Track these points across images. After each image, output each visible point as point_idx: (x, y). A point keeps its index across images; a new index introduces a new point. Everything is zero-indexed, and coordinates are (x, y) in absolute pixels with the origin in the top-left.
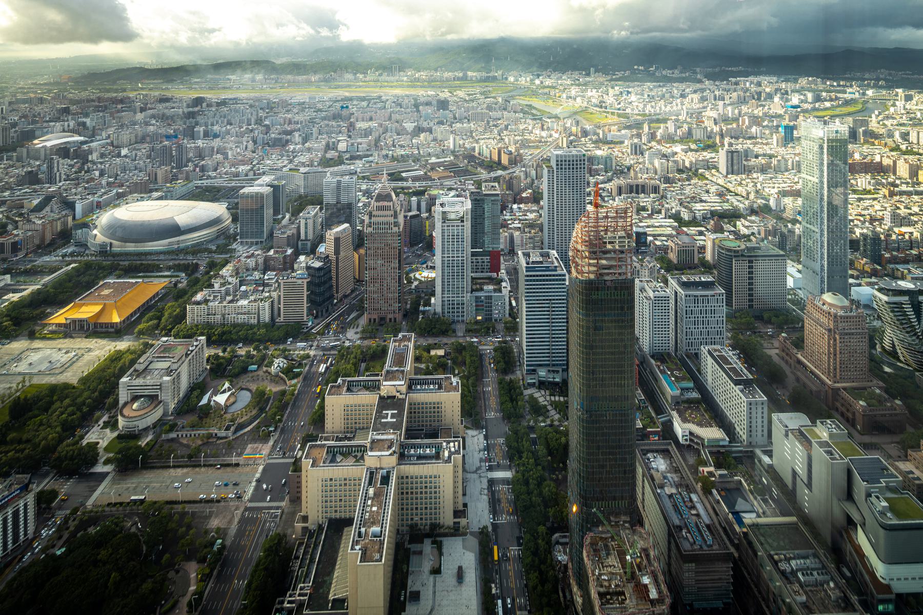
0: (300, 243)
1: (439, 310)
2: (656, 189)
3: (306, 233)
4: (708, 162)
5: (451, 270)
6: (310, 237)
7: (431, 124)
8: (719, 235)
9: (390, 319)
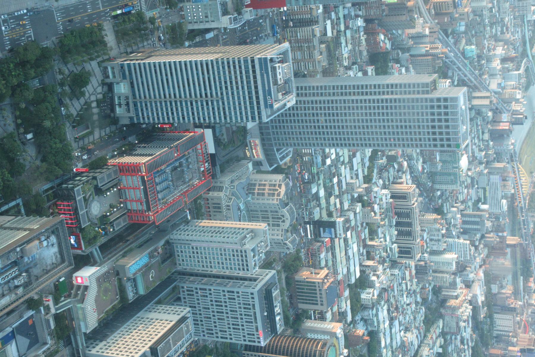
2: (405, 252)
4: (456, 334)
8: (342, 342)
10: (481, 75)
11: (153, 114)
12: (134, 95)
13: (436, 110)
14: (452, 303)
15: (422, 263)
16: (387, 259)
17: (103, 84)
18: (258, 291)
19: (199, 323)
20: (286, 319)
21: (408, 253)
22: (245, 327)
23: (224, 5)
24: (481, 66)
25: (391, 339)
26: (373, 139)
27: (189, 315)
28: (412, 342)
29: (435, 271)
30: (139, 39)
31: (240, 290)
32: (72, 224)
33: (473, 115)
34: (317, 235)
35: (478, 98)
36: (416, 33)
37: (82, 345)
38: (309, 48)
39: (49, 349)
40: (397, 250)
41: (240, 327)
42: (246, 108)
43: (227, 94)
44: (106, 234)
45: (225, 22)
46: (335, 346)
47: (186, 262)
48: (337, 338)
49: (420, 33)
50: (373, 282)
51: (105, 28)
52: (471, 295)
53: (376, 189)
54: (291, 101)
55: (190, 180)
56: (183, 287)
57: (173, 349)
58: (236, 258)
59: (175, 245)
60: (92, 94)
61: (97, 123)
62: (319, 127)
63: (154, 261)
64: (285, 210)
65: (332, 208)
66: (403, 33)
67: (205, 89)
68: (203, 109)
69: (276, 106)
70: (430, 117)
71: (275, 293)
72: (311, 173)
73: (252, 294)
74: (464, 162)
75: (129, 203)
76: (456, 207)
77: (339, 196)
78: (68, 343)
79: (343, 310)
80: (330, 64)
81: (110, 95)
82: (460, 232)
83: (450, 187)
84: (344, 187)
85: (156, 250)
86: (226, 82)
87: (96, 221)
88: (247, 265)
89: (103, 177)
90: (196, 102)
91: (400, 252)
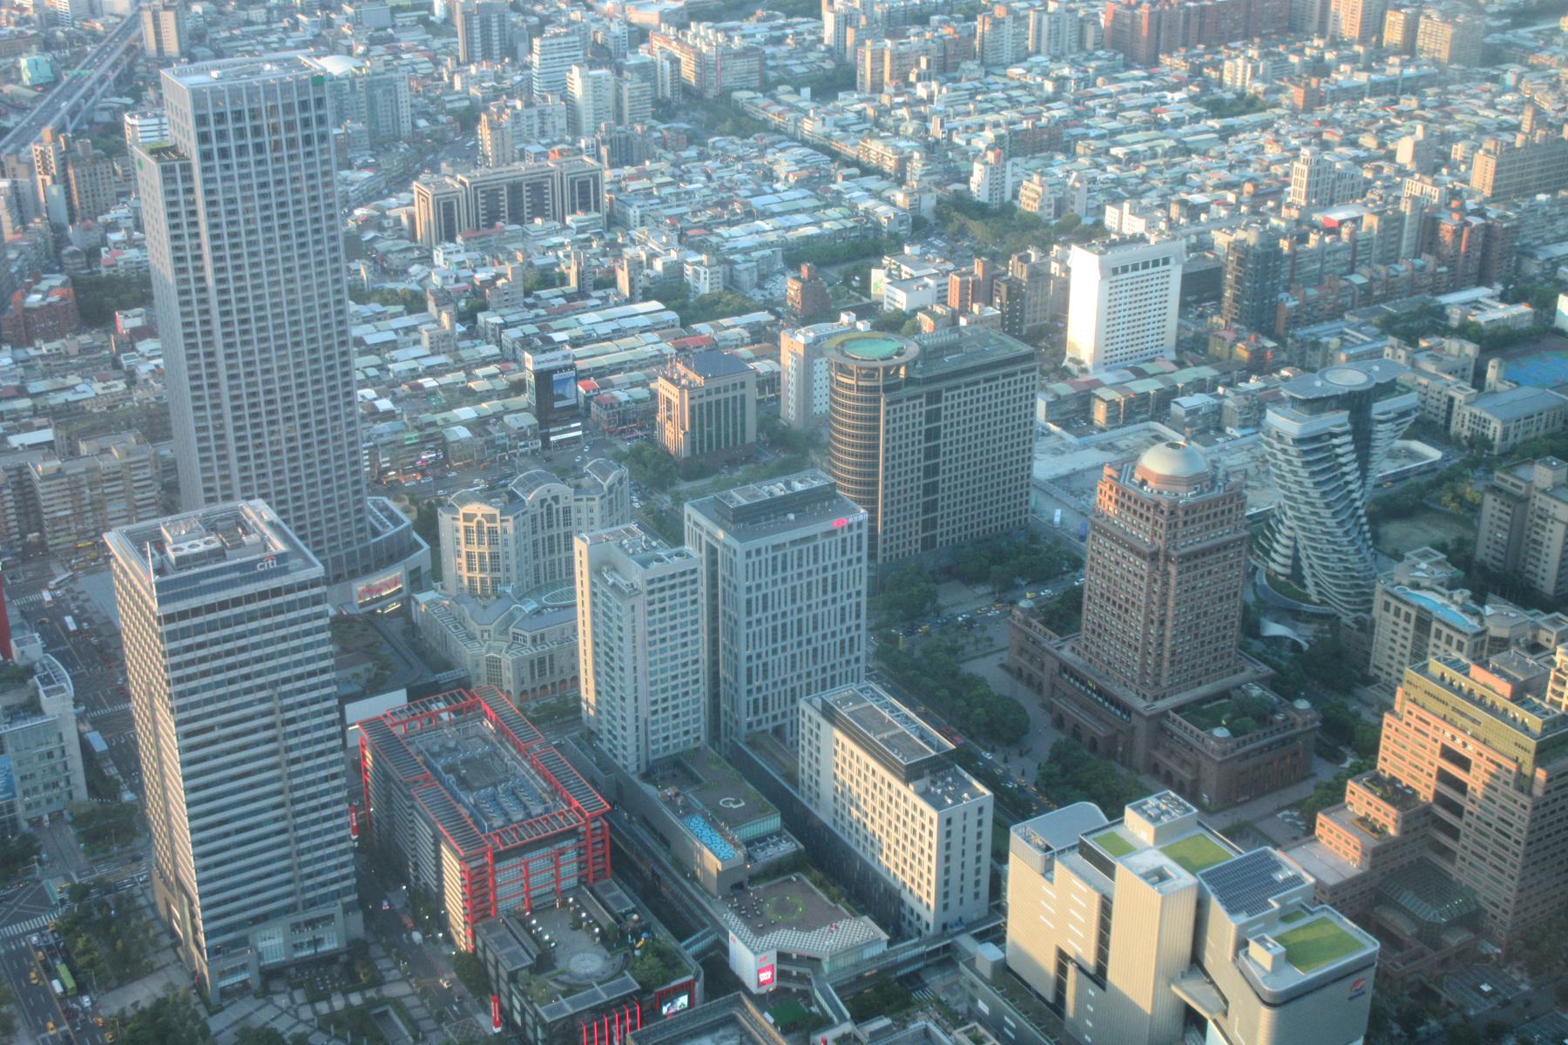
4: (763, 58)
8: (825, 328)
10: (96, 37)
11: (330, 857)
12: (292, 909)
13: (232, 143)
14: (688, 72)
15: (604, 151)
16: (608, 236)
17: (265, 993)
18: (741, 540)
19: (829, 673)
20: (786, 469)
21: (584, 186)
22: (829, 563)
23: (13, 714)
24: (71, 39)
25: (797, 211)
26: (322, 296)
27: (818, 702)
28: (798, 162)
29: (619, 118)
30: (133, 922)
31: (743, 585)
32: (633, 1015)
33: (208, 52)
34: (575, 412)
35: (159, 41)
36: (10, 211)
37: (916, 945)
38: (93, 485)
39: (937, 1022)
40: (580, 215)
41: (829, 574)
42: (293, 622)
43: (259, 674)
44: (647, 929)
45: (59, 705)
46: (842, 344)
47: (685, 726)
48: (817, 340)
49: (8, 202)
50: (666, 266)
51: (115, 1010)
52: (663, 27)
53: (436, 280)
54: (259, 512)
55: (485, 741)
56: (750, 725)
57: (902, 728)
58: (667, 603)
59: (652, 758)
60: (296, 1016)
61: (370, 993)
62: (306, 436)
63: (697, 803)
64: (529, 498)
65: (501, 383)
66: (14, 247)
67: (254, 731)
68: (305, 731)
69: (279, 546)
70: (251, 157)
71: (739, 498)
72: (421, 446)
73: (748, 555)
74: (335, 66)
75: (565, 884)
76: (451, 78)
77: (469, 369)
78: (914, 980)
79: (746, 334)
80: (129, 427)
81: (293, 971)
82: (512, 64)
83: (404, 96)
84: (442, 359)
85: (670, 802)
86: (231, 681)
87: (619, 959)
88: (683, 574)
89: (506, 959)
90: (289, 749)
91: (585, 206)
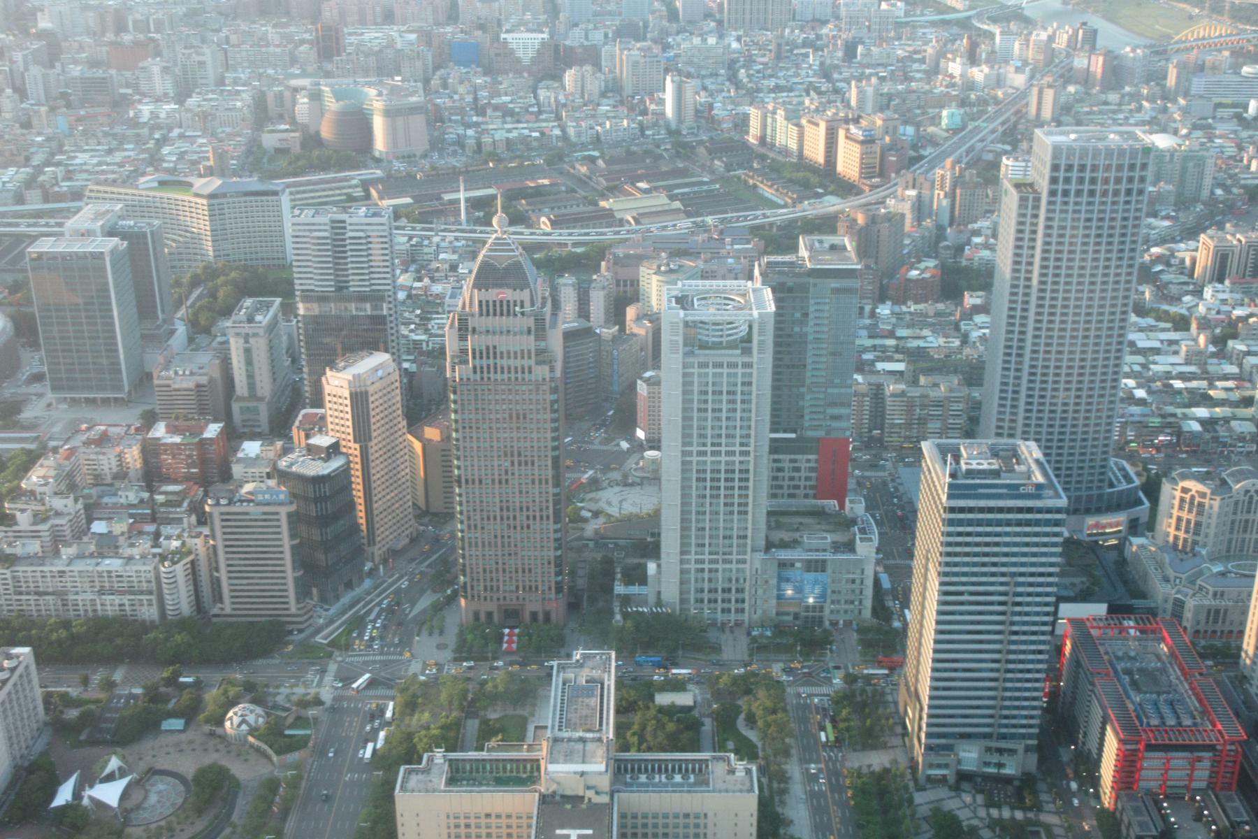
0: (235, 407)
1: (671, 593)
3: (250, 376)
5: (712, 485)
6: (265, 386)
7: (597, 37)
9: (534, 615)
